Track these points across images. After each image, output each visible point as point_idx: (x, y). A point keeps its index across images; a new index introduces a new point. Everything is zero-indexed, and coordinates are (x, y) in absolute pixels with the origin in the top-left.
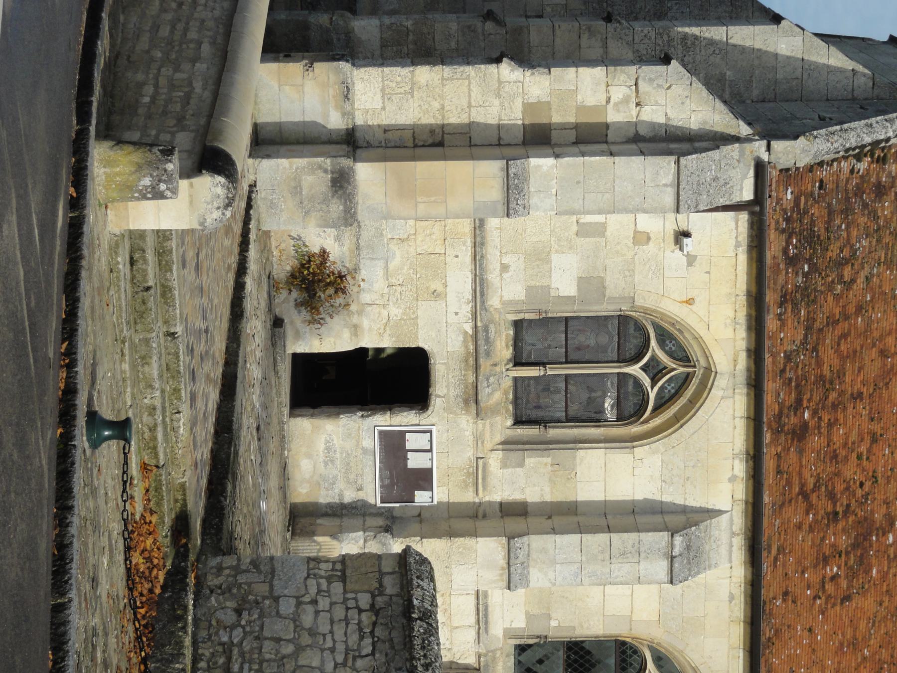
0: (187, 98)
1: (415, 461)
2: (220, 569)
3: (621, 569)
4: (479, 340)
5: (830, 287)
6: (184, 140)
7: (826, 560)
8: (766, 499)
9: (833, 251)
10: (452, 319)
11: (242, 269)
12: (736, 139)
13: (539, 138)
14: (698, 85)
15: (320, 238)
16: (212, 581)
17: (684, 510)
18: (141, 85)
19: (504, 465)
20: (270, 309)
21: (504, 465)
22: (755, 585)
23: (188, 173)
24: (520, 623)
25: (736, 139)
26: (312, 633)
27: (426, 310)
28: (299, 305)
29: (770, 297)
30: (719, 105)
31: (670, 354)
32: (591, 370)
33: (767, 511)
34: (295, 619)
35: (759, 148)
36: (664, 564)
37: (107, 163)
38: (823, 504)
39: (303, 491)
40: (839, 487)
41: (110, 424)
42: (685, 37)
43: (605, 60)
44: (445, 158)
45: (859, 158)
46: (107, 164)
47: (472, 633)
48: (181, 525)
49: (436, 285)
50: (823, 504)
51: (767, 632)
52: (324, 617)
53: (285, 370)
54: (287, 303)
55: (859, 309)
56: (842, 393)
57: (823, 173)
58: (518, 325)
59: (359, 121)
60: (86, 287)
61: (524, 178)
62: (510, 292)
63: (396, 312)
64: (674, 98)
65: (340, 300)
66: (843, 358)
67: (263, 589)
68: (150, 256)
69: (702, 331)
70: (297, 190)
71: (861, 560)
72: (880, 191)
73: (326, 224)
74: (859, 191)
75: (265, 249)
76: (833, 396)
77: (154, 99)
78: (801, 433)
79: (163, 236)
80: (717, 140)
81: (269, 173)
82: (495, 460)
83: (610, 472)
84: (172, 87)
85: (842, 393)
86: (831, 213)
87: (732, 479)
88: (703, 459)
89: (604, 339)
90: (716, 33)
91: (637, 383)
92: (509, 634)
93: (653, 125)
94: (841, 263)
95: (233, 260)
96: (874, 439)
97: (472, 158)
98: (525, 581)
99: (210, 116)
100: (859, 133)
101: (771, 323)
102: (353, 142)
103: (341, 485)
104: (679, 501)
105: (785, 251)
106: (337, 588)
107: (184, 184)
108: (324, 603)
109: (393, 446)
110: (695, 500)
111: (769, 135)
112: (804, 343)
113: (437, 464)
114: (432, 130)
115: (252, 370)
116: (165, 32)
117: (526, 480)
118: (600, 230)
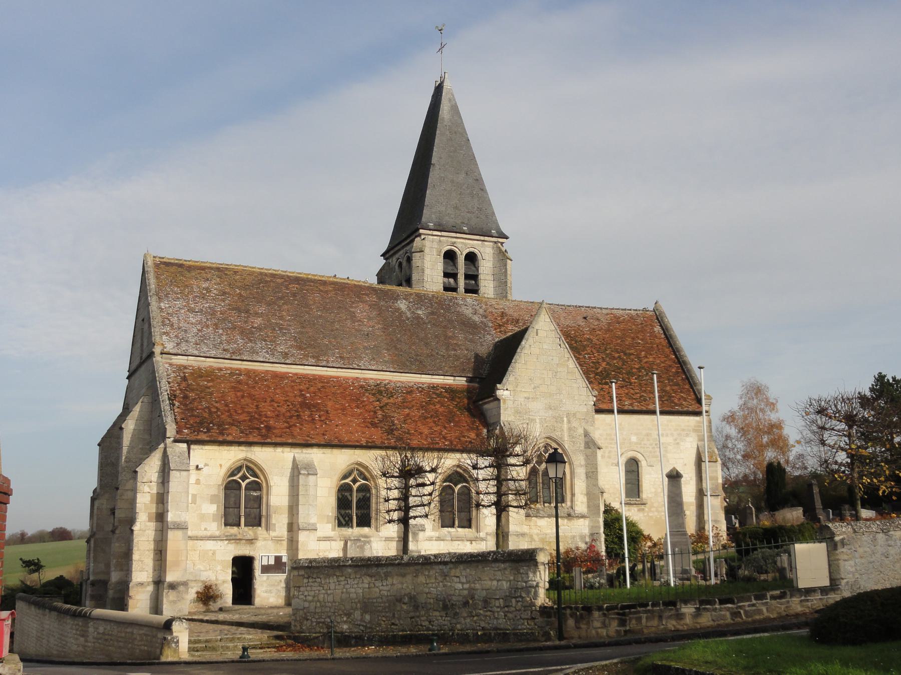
0: (146, 635)
1: (272, 562)
2: (295, 626)
3: (312, 491)
4: (230, 539)
5: (218, 416)
6: (160, 635)
7: (314, 419)
8: (290, 441)
9: (206, 415)
10: (223, 548)
11: (202, 621)
12: (165, 449)
13: (160, 517)
14: (145, 462)
15: (192, 594)
16: (298, 628)
17: (293, 469)
18: (140, 650)
19: (275, 530)
20: (215, 612)
21: (275, 530)
22: (319, 446)
23: (171, 633)
24: (330, 526)
25: (165, 449)
26: (314, 597)
27: (219, 557)
28: (215, 602)
29: (221, 439)
30: (153, 454)
31: (239, 472)
32: (243, 501)
33: (295, 441)
34: (310, 602)
35: (168, 441)
36: (310, 477)
37: (167, 657)
38: (294, 420)
39: (281, 601)
40: (288, 414)
41: (244, 652)
42: (126, 461)
43: (134, 490)
44: (166, 550)
45: (174, 405)
46: (168, 656)
47: (333, 542)
48: (277, 637)
49: (210, 554)
50: (294, 420)
51: (336, 442)
52: (310, 593)
53: (237, 607)
54: (214, 606)
55: (227, 405)
56: (256, 413)
57: (178, 418)
58: (226, 525)
59: (151, 580)
60: (204, 660)
61: (174, 523)
62: (215, 527)
63: (219, 568)
64: (150, 470)
65: (214, 587)
66: (244, 412)
67: (301, 612)
68: (196, 645)
69: (231, 462)
70: (174, 602)
71: (314, 406)
72: (186, 397)
73: (187, 592)
74: (186, 405)
75: (194, 613)
76: (256, 416)
77: (145, 645)
78: (269, 428)
79: (190, 642)
80: (165, 456)
81: (168, 612)
82: (273, 534)
83: (277, 495)
84: (141, 640)
85: (256, 413)
86: (193, 416)
87: (283, 452)
88: (277, 462)
89: (233, 495)
90: (125, 450)
91: (247, 484)
92: (333, 530)
93: (158, 477)
94: (210, 413)
95: (198, 623)
96: (272, 401)
97: (167, 541)
98: (314, 524)
99: (153, 627)
100: (165, 405)
101: (230, 438)
102: (158, 582)
103: (279, 588)
104: (290, 470)
105: (205, 433)
106: (302, 589)
107: (175, 634)
108: (306, 593)
109: (266, 569)
110: (290, 465)
111: (164, 437)
112: (237, 426)
113: (273, 555)
114: (156, 554)
115: (236, 617)
116: (121, 644)
117: (280, 522)
118: (194, 496)
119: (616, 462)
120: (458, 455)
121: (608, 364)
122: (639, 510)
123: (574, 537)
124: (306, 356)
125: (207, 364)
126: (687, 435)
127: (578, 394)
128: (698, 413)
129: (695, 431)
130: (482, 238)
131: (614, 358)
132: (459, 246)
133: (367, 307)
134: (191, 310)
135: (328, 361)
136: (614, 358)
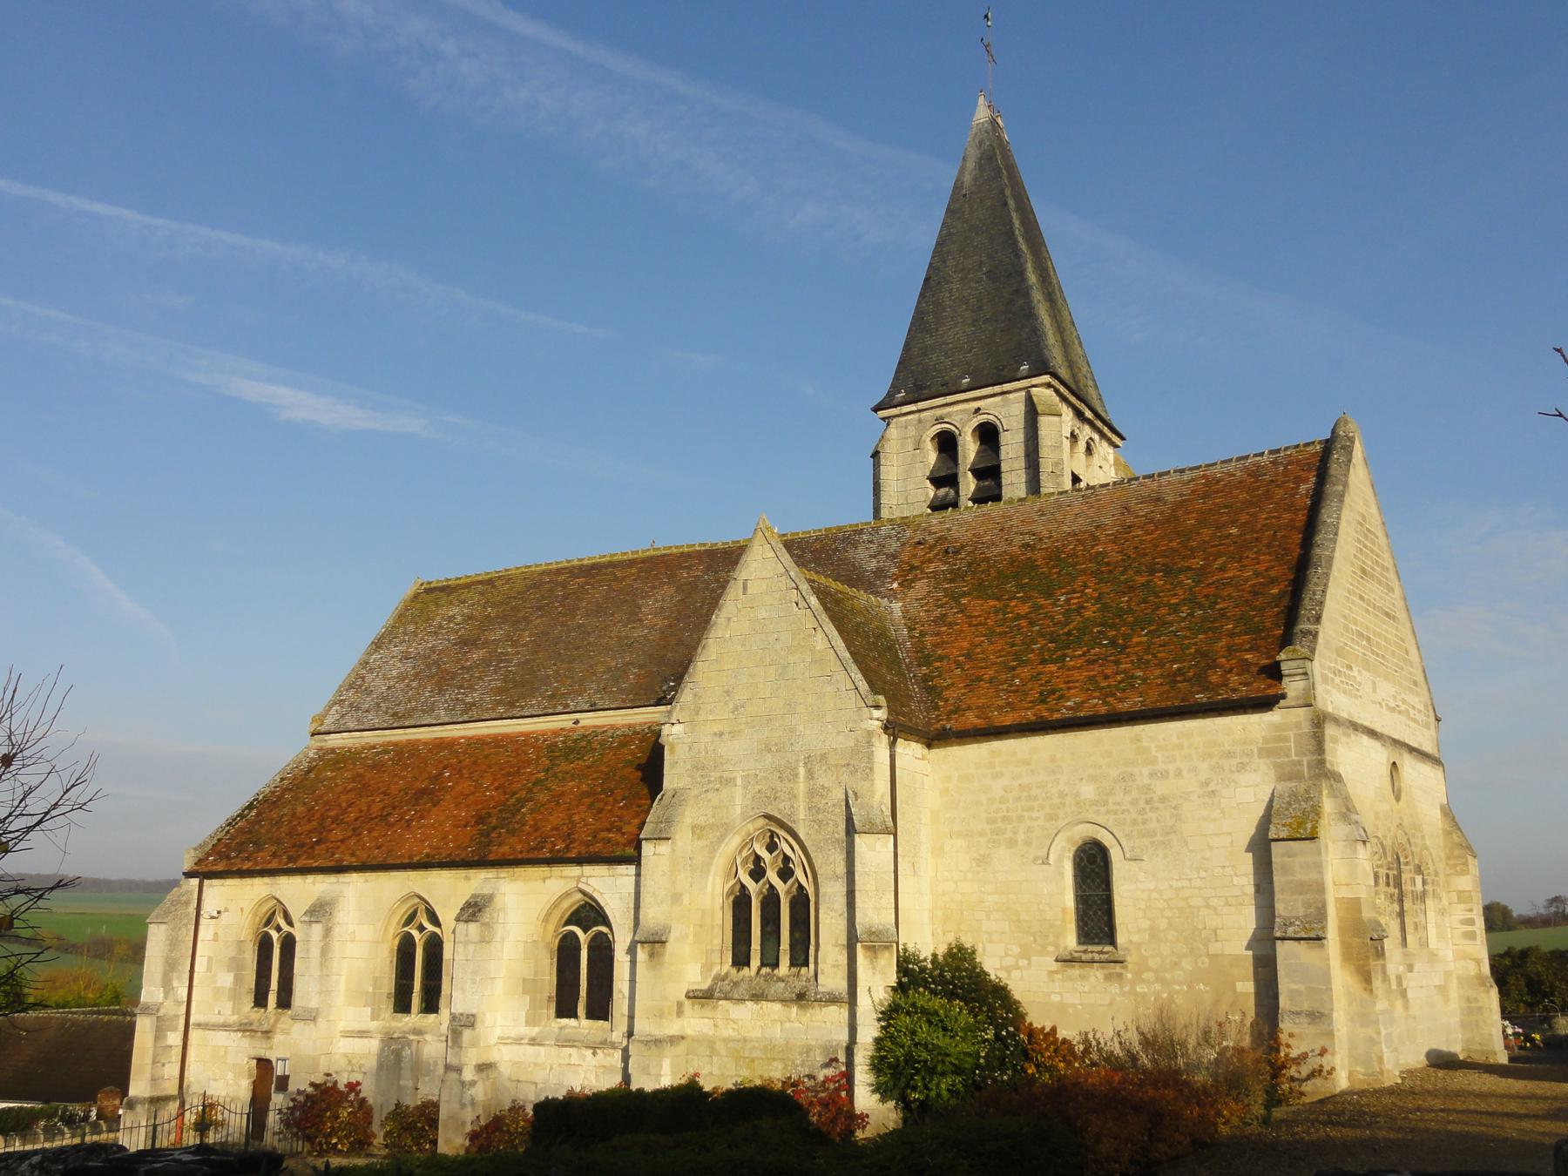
4: (245, 1028)
32: (273, 970)
119: (1042, 853)
120: (574, 871)
121: (1105, 608)
122: (1108, 978)
123: (808, 1050)
124: (498, 703)
125: (363, 742)
126: (1242, 768)
127: (834, 708)
128: (1265, 704)
129: (1265, 752)
130: (997, 389)
131: (1132, 589)
132: (956, 419)
133: (673, 589)
134: (405, 657)
135: (568, 706)
136: (1132, 589)
